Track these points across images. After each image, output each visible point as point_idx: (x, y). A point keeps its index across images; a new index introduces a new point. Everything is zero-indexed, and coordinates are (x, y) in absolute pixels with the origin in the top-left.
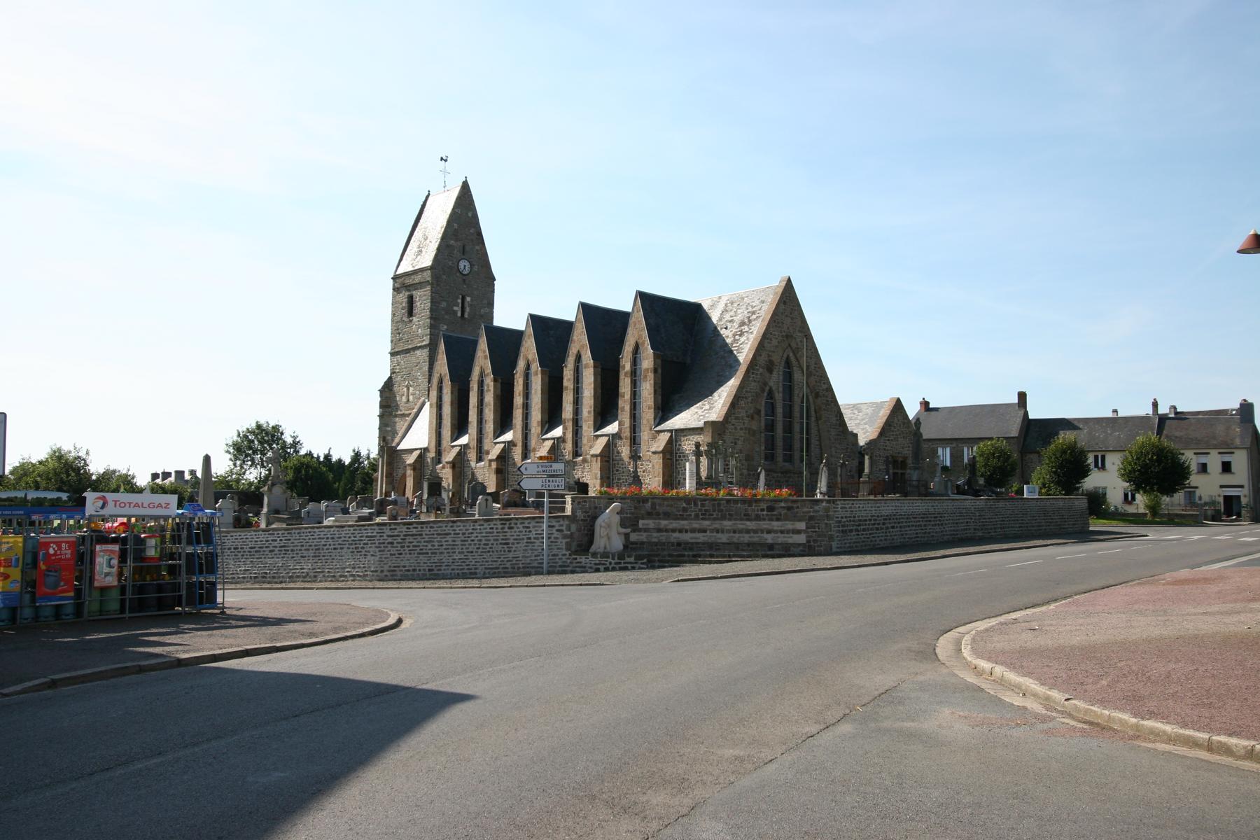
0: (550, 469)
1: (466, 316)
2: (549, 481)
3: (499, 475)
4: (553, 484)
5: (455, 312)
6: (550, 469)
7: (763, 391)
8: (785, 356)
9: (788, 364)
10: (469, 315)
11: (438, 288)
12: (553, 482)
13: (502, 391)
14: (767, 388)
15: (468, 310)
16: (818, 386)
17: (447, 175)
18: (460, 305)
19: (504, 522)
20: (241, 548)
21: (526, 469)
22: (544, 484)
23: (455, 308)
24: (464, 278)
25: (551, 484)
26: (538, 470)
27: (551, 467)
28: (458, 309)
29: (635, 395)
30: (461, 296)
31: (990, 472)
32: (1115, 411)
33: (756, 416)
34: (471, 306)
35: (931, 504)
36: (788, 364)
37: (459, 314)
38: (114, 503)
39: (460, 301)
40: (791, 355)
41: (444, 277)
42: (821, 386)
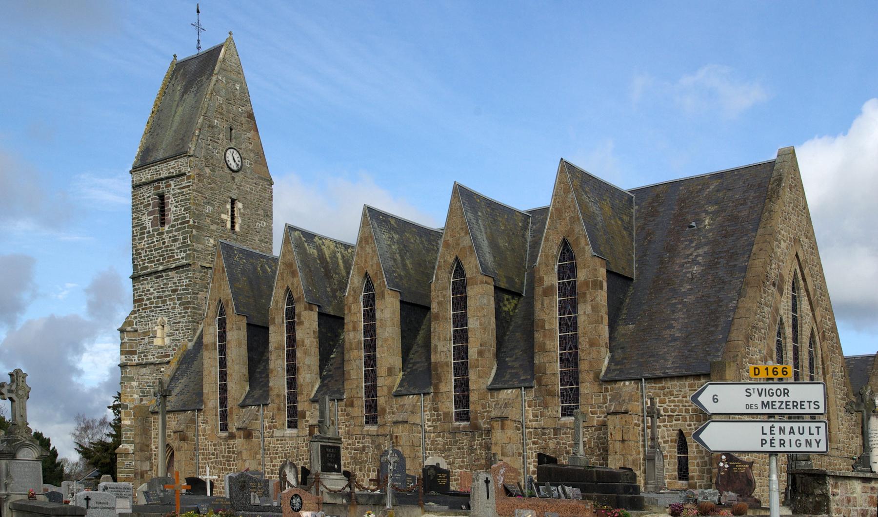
0: (784, 399)
1: (237, 228)
2: (782, 430)
4: (794, 438)
5: (223, 222)
6: (784, 399)
7: (775, 321)
10: (241, 227)
11: (201, 185)
12: (792, 431)
13: (319, 325)
15: (238, 221)
17: (202, 33)
18: (230, 214)
20: (179, 283)
21: (715, 399)
22: (768, 437)
23: (224, 216)
24: (233, 174)
25: (787, 437)
26: (750, 401)
27: (786, 393)
28: (226, 217)
29: (569, 324)
30: (230, 200)
34: (243, 215)
37: (229, 226)
38: (764, 432)
39: (229, 206)
41: (207, 170)
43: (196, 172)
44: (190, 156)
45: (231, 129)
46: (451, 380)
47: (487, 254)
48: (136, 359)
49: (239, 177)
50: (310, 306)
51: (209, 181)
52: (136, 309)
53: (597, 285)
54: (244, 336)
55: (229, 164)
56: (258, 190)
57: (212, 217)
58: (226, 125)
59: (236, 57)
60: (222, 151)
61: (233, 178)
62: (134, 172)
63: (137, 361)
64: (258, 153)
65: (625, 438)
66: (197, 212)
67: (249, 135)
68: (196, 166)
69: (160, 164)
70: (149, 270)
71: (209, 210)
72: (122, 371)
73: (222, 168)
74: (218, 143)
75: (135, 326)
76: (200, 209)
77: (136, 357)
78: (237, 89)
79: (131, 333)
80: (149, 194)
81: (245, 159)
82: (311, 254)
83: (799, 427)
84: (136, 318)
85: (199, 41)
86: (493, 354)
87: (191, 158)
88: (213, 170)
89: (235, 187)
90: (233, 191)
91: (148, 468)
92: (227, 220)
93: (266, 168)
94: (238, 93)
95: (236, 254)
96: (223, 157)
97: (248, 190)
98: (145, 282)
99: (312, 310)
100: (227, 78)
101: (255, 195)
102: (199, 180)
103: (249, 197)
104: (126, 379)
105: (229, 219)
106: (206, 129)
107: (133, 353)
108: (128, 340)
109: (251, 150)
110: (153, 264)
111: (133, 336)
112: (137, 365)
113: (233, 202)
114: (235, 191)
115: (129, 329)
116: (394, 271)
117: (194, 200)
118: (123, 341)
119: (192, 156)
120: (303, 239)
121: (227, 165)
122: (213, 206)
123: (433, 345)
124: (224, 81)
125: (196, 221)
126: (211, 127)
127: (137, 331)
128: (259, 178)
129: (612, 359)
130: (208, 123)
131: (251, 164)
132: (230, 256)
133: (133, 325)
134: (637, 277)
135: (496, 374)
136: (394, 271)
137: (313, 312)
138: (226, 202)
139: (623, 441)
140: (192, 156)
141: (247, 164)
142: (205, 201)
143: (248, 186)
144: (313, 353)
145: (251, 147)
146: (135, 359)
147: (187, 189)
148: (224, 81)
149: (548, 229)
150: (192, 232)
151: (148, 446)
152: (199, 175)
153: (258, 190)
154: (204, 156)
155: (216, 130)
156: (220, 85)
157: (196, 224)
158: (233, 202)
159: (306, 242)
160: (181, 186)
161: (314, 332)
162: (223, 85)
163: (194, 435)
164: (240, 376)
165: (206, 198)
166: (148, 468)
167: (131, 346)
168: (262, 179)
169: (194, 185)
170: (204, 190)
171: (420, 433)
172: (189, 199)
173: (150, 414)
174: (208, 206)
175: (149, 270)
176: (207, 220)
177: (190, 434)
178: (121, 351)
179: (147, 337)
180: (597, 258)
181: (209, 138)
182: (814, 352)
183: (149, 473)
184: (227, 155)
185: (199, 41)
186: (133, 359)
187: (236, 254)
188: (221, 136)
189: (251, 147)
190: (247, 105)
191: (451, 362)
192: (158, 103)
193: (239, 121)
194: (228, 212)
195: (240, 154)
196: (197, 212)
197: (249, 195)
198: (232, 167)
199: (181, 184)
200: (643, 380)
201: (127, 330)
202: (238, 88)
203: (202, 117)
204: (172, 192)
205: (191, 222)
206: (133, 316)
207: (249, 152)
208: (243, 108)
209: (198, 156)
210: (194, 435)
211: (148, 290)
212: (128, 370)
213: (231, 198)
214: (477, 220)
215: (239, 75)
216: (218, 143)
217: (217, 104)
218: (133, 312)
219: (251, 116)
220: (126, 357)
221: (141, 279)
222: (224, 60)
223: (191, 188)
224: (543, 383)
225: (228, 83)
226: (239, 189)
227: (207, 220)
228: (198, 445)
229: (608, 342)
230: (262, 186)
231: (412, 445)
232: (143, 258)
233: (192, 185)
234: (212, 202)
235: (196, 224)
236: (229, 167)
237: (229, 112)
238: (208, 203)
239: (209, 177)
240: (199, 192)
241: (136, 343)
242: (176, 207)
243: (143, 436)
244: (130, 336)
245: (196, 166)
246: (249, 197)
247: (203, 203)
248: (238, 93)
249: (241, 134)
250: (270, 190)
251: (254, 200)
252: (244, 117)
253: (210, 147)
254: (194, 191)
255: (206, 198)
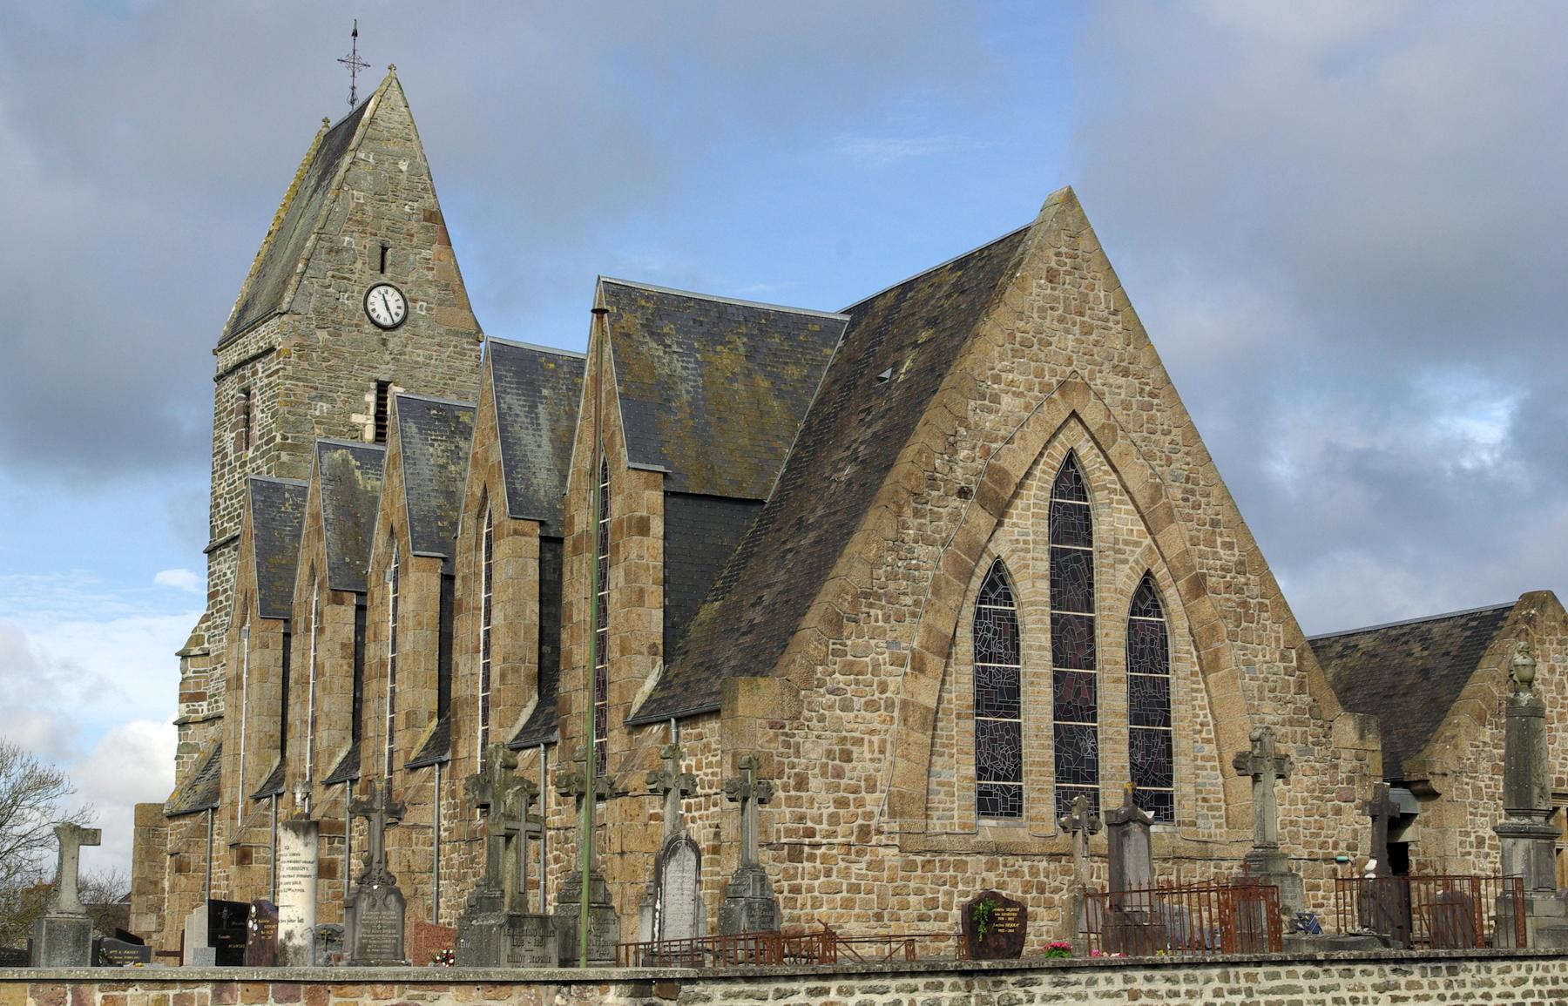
3: (325, 882)
5: (356, 430)
8: (1058, 452)
9: (1071, 479)
11: (305, 365)
14: (986, 563)
16: (1202, 555)
18: (372, 410)
19: (819, 984)
23: (356, 418)
24: (385, 335)
30: (373, 385)
31: (604, 862)
32: (326, 121)
33: (934, 662)
35: (1376, 979)
36: (1071, 479)
39: (371, 398)
40: (1085, 450)
41: (322, 335)
42: (1216, 556)
43: (293, 342)
44: (282, 314)
45: (384, 249)
46: (475, 731)
47: (543, 475)
48: (205, 708)
49: (395, 340)
50: (335, 596)
51: (325, 355)
52: (210, 612)
53: (643, 527)
54: (277, 659)
55: (374, 315)
56: (444, 356)
57: (329, 424)
58: (371, 243)
59: (403, 109)
60: (360, 292)
61: (384, 342)
62: (220, 350)
63: (206, 713)
64: (447, 285)
65: (625, 849)
66: (292, 418)
67: (425, 253)
68: (295, 330)
69: (248, 332)
70: (228, 535)
71: (321, 411)
72: (180, 735)
73: (356, 325)
74: (349, 280)
75: (206, 645)
76: (301, 410)
77: (205, 704)
78: (401, 171)
79: (199, 659)
80: (232, 387)
81: (415, 301)
82: (367, 492)
83: (299, 855)
84: (208, 629)
85: (353, 88)
86: (527, 676)
87: (285, 318)
88: (336, 333)
89: (387, 358)
90: (383, 367)
91: (153, 927)
92: (364, 425)
93: (466, 312)
94: (403, 177)
95: (288, 500)
96: (361, 305)
97: (421, 359)
98: (222, 558)
99: (341, 603)
100: (377, 153)
101: (436, 367)
102: (300, 357)
103: (420, 374)
104: (186, 749)
105: (371, 421)
106: (323, 257)
107: (199, 697)
108: (194, 672)
109: (431, 282)
110: (232, 524)
111: (201, 664)
112: (205, 720)
113: (382, 388)
114: (390, 366)
115: (196, 651)
116: (441, 518)
117: (287, 395)
118: (185, 676)
119: (285, 313)
120: (354, 462)
121: (370, 318)
122: (332, 401)
123: (454, 663)
124: (371, 160)
125: (289, 435)
126: (335, 251)
127: (208, 654)
128: (449, 332)
129: (663, 683)
130: (327, 244)
131: (428, 309)
132: (272, 505)
133: (203, 643)
134: (772, 502)
135: (533, 719)
136: (441, 518)
137: (343, 608)
138: (366, 390)
139: (622, 853)
140: (285, 313)
141: (419, 309)
142: (314, 393)
143: (421, 352)
144: (336, 688)
145: (430, 275)
146: (204, 708)
147: (276, 377)
148: (371, 160)
149: (583, 419)
150: (278, 457)
151: (155, 883)
152: (301, 347)
153: (444, 356)
154: (315, 310)
155: (345, 255)
156: (362, 169)
157: (289, 441)
158: (382, 388)
159: (358, 468)
160: (270, 371)
161: (343, 646)
162: (368, 169)
163: (205, 860)
164: (260, 739)
165: (316, 389)
166: (153, 927)
167: (198, 685)
168: (456, 334)
169: (289, 368)
170: (312, 373)
171: (432, 845)
172: (276, 396)
173: (165, 819)
174: (320, 404)
175: (228, 535)
176: (317, 431)
177: (195, 858)
178: (181, 695)
179: (219, 665)
180: (634, 472)
181: (330, 273)
182: (1167, 624)
183: (154, 937)
184: (371, 299)
185: (353, 88)
186: (200, 709)
187: (288, 500)
188: (359, 265)
189: (430, 275)
190: (426, 196)
191: (475, 697)
192: (283, 215)
193: (405, 231)
194: (367, 408)
195: (401, 294)
196: (292, 418)
197: (423, 370)
198: (381, 321)
199: (269, 369)
200: (673, 721)
201: (192, 654)
202: (404, 168)
203: (313, 236)
204: (259, 385)
205: (278, 439)
206: (204, 626)
207: (426, 286)
208: (416, 204)
209: (300, 311)
210: (205, 860)
211: (225, 575)
212: (190, 732)
213: (377, 381)
214: (533, 407)
215: (409, 144)
216: (349, 280)
217: (353, 205)
218: (206, 618)
219: (434, 217)
220: (188, 706)
221: (218, 552)
222: (372, 120)
223: (280, 373)
224: (568, 736)
225: (379, 162)
226: (398, 360)
227: (317, 431)
228: (210, 879)
229: (659, 641)
230: (455, 347)
231: (406, 869)
232: (222, 513)
233: (284, 369)
234: (331, 394)
235: (289, 441)
236: (373, 322)
237: (379, 216)
238: (321, 398)
239: (326, 348)
240: (298, 379)
241: (207, 678)
242: (262, 411)
243: (146, 864)
244: (196, 665)
245: (295, 330)
246: (420, 374)
247: (309, 398)
248: (403, 177)
249: (407, 255)
250: (473, 354)
251: (434, 377)
252: (418, 221)
253: (331, 290)
254: (287, 377)
255: (316, 389)
